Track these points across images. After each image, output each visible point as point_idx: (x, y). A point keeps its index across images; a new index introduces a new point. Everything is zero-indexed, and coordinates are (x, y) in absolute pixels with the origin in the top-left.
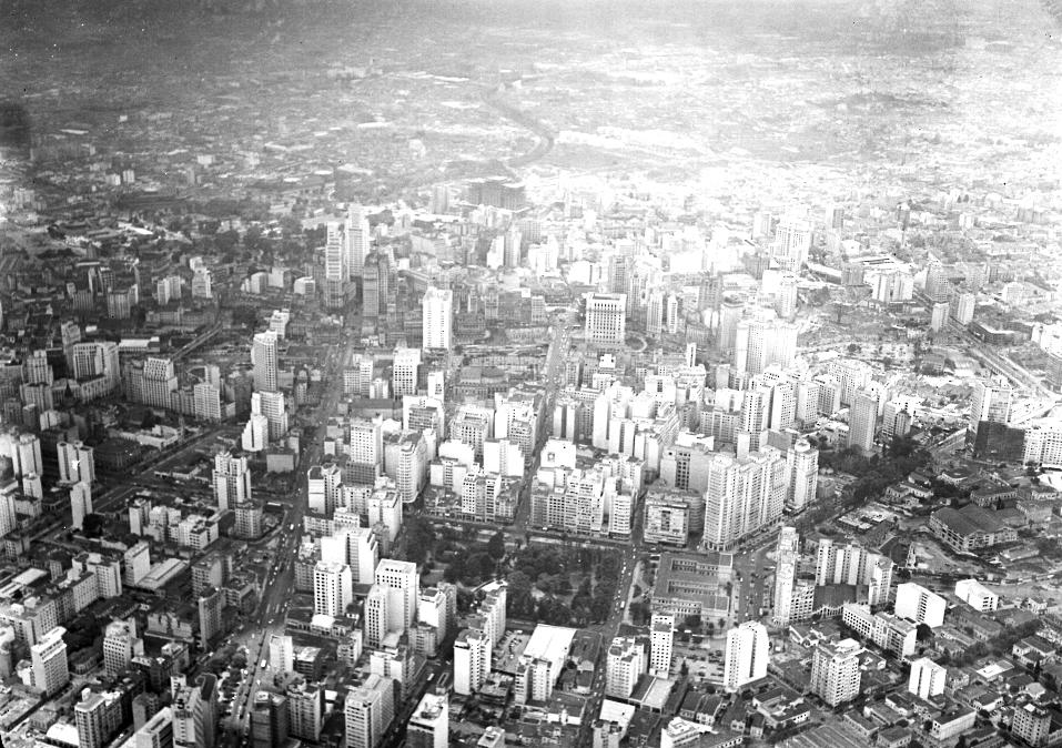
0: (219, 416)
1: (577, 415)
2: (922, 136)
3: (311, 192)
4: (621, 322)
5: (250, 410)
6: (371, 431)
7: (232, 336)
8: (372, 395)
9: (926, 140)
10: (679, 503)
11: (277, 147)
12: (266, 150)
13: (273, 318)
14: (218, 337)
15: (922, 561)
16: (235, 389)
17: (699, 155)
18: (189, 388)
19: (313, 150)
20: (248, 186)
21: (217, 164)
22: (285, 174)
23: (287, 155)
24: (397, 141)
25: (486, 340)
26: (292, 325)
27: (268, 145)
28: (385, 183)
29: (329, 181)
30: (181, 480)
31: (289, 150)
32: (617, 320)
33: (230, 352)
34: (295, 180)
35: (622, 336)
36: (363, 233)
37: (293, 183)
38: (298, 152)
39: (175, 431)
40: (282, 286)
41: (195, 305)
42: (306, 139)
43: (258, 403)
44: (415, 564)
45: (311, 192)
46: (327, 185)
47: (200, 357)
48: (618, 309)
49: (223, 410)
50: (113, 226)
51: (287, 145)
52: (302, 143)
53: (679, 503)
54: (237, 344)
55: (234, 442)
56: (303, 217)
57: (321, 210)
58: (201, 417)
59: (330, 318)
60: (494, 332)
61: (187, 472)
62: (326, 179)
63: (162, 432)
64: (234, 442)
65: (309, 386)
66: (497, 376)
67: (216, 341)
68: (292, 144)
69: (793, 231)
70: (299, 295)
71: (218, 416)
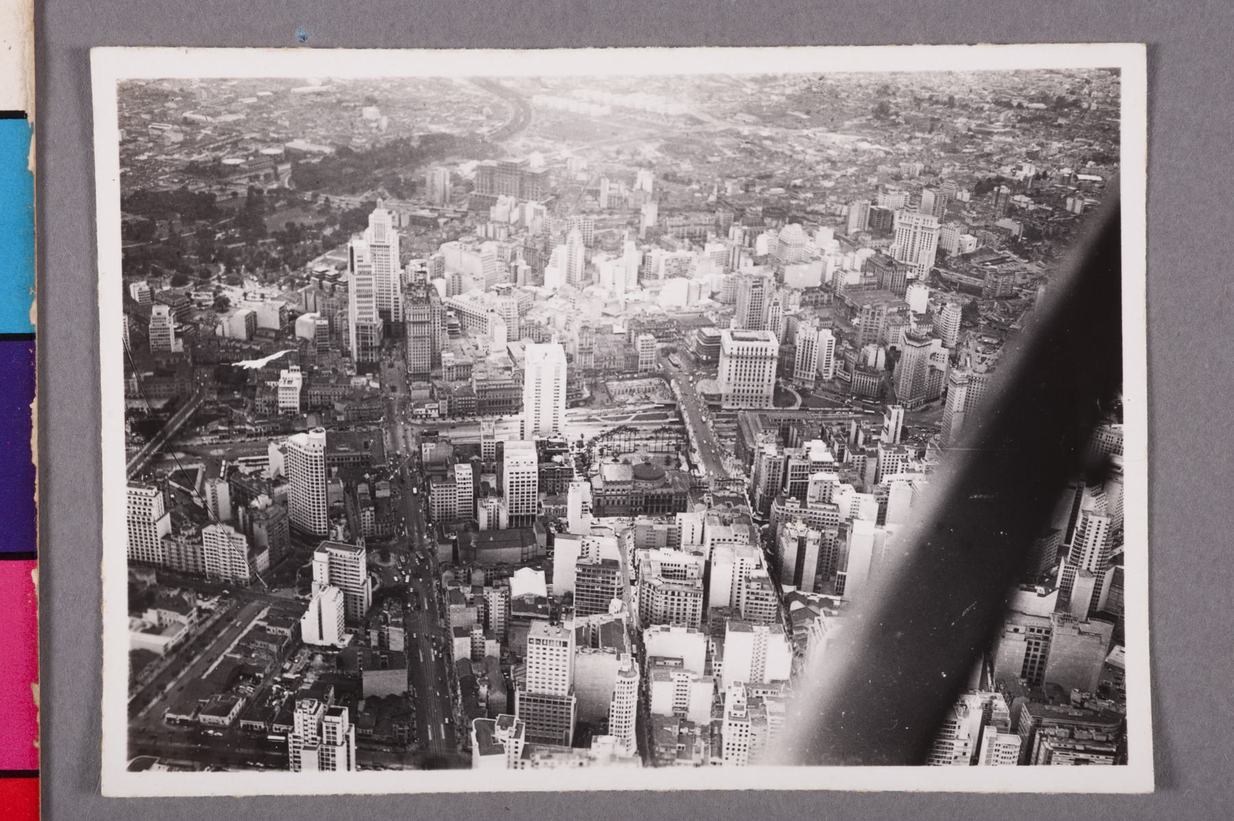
0: (248, 576)
1: (821, 555)
2: (930, 98)
3: (262, 178)
4: (771, 368)
5: (311, 579)
6: (565, 644)
7: (220, 410)
8: (483, 522)
9: (937, 102)
10: (1100, 743)
11: (203, 118)
12: (186, 122)
13: (281, 384)
14: (202, 412)
15: (578, 392)
16: (269, 528)
17: (700, 122)
18: (192, 531)
19: (246, 121)
20: (177, 171)
21: (130, 142)
22: (221, 154)
23: (215, 128)
24: (346, 108)
25: (585, 401)
26: (310, 392)
27: (188, 114)
28: (353, 165)
29: (282, 162)
30: (216, 727)
31: (216, 121)
32: (767, 369)
33: (223, 438)
34: (238, 161)
35: (769, 390)
36: (391, 249)
37: (236, 166)
38: (229, 124)
39: (184, 619)
40: (277, 326)
41: (157, 363)
42: (233, 107)
43: (325, 567)
44: (173, 350)
45: (262, 178)
46: (281, 168)
47: (179, 449)
48: (769, 354)
49: (252, 564)
50: (284, 696)
51: (213, 116)
52: (231, 113)
53: (1100, 743)
54: (231, 423)
55: (287, 632)
56: (263, 213)
57: (282, 203)
58: (215, 577)
59: (363, 380)
60: (593, 387)
61: (225, 711)
62: (277, 160)
63: (160, 618)
64: (287, 632)
65: (376, 506)
66: (657, 479)
67: (201, 420)
68: (219, 114)
69: (919, 229)
70: (305, 341)
71: (246, 575)
